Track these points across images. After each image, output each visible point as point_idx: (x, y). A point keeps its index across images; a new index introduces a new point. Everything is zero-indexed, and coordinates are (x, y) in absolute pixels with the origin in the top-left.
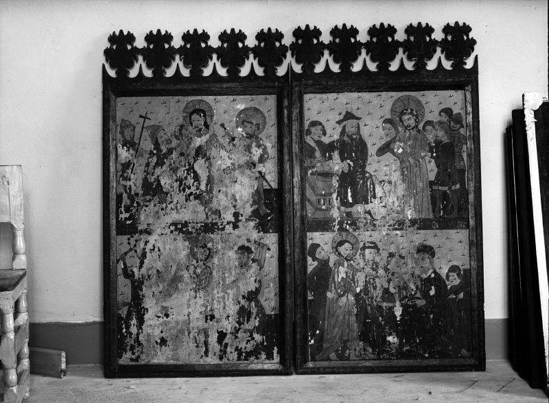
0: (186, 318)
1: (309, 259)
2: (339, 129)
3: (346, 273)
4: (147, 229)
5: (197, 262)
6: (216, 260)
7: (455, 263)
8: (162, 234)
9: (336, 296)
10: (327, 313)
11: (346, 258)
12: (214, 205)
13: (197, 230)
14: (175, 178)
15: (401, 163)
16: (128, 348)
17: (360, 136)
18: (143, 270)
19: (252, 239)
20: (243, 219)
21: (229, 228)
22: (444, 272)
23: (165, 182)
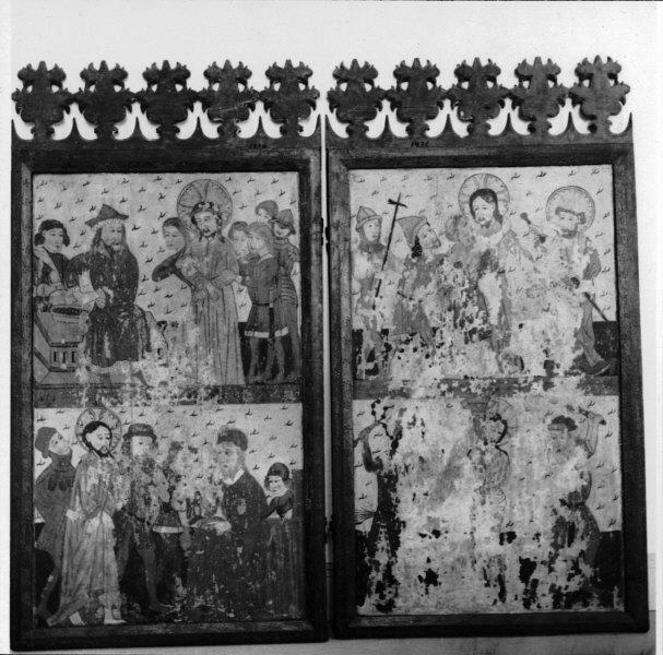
0: (469, 537)
1: (38, 455)
2: (91, 234)
3: (100, 477)
4: (402, 389)
5: (486, 444)
6: (516, 441)
7: (282, 460)
8: (428, 397)
9: (82, 517)
10: (66, 547)
11: (99, 452)
12: (513, 348)
13: (484, 390)
14: (447, 304)
15: (193, 291)
16: (373, 588)
17: (127, 246)
18: (398, 457)
19: (575, 406)
20: (560, 372)
21: (538, 387)
22: (260, 476)
23: (431, 307)
